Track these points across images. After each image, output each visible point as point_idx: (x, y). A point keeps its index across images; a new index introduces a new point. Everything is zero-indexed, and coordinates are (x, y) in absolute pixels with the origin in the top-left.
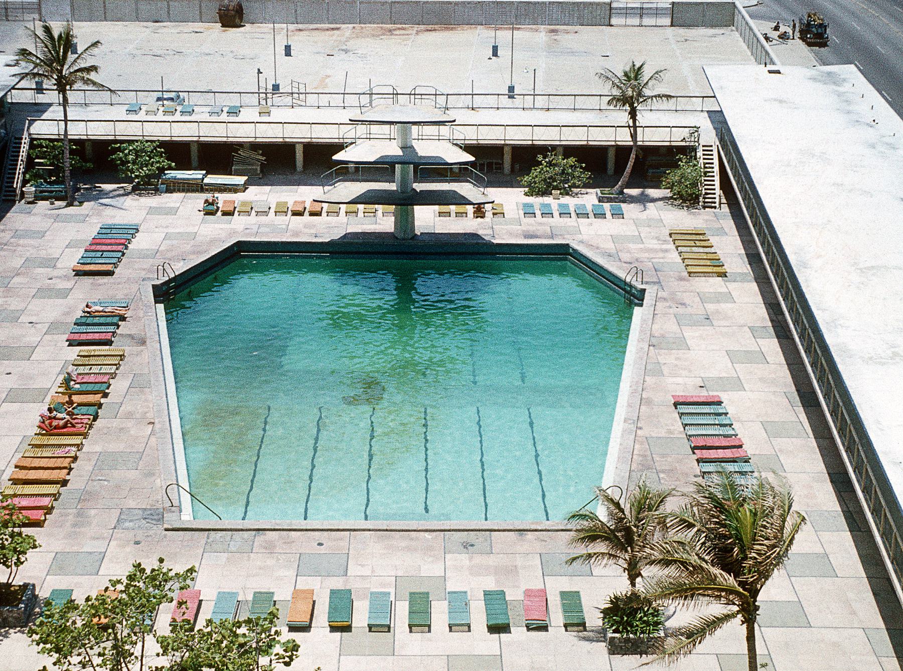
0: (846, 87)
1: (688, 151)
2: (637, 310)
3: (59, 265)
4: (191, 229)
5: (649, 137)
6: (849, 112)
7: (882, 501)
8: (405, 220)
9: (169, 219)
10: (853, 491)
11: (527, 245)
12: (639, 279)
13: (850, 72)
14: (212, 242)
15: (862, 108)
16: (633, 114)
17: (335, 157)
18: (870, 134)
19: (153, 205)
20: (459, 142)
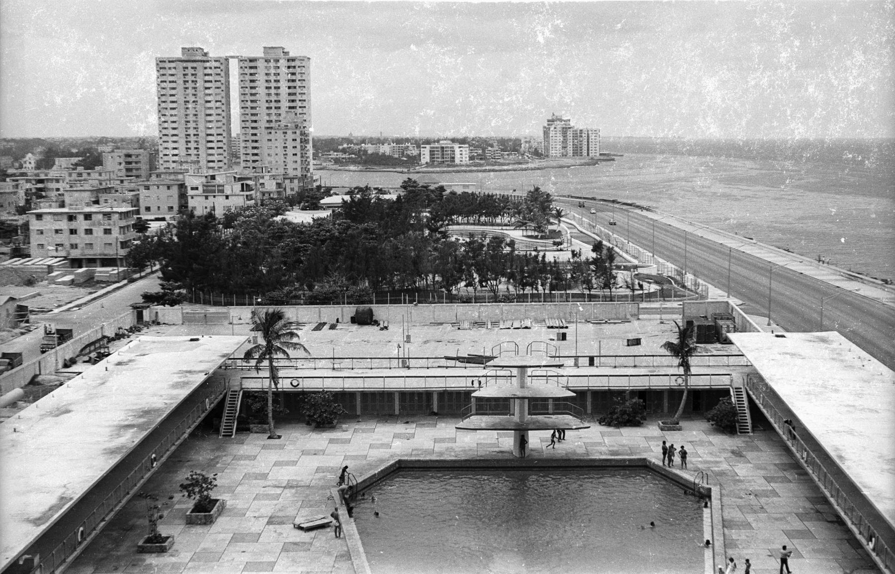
0: (835, 345)
1: (725, 392)
2: (706, 512)
3: (269, 477)
4: (365, 453)
5: (695, 382)
6: (842, 361)
7: (683, 401)
8: (522, 442)
9: (346, 446)
10: (681, 400)
11: (614, 460)
12: (705, 481)
13: (834, 335)
14: (382, 461)
15: (848, 357)
16: (685, 365)
17: (575, 395)
18: (862, 374)
19: (332, 437)
20: (572, 388)
